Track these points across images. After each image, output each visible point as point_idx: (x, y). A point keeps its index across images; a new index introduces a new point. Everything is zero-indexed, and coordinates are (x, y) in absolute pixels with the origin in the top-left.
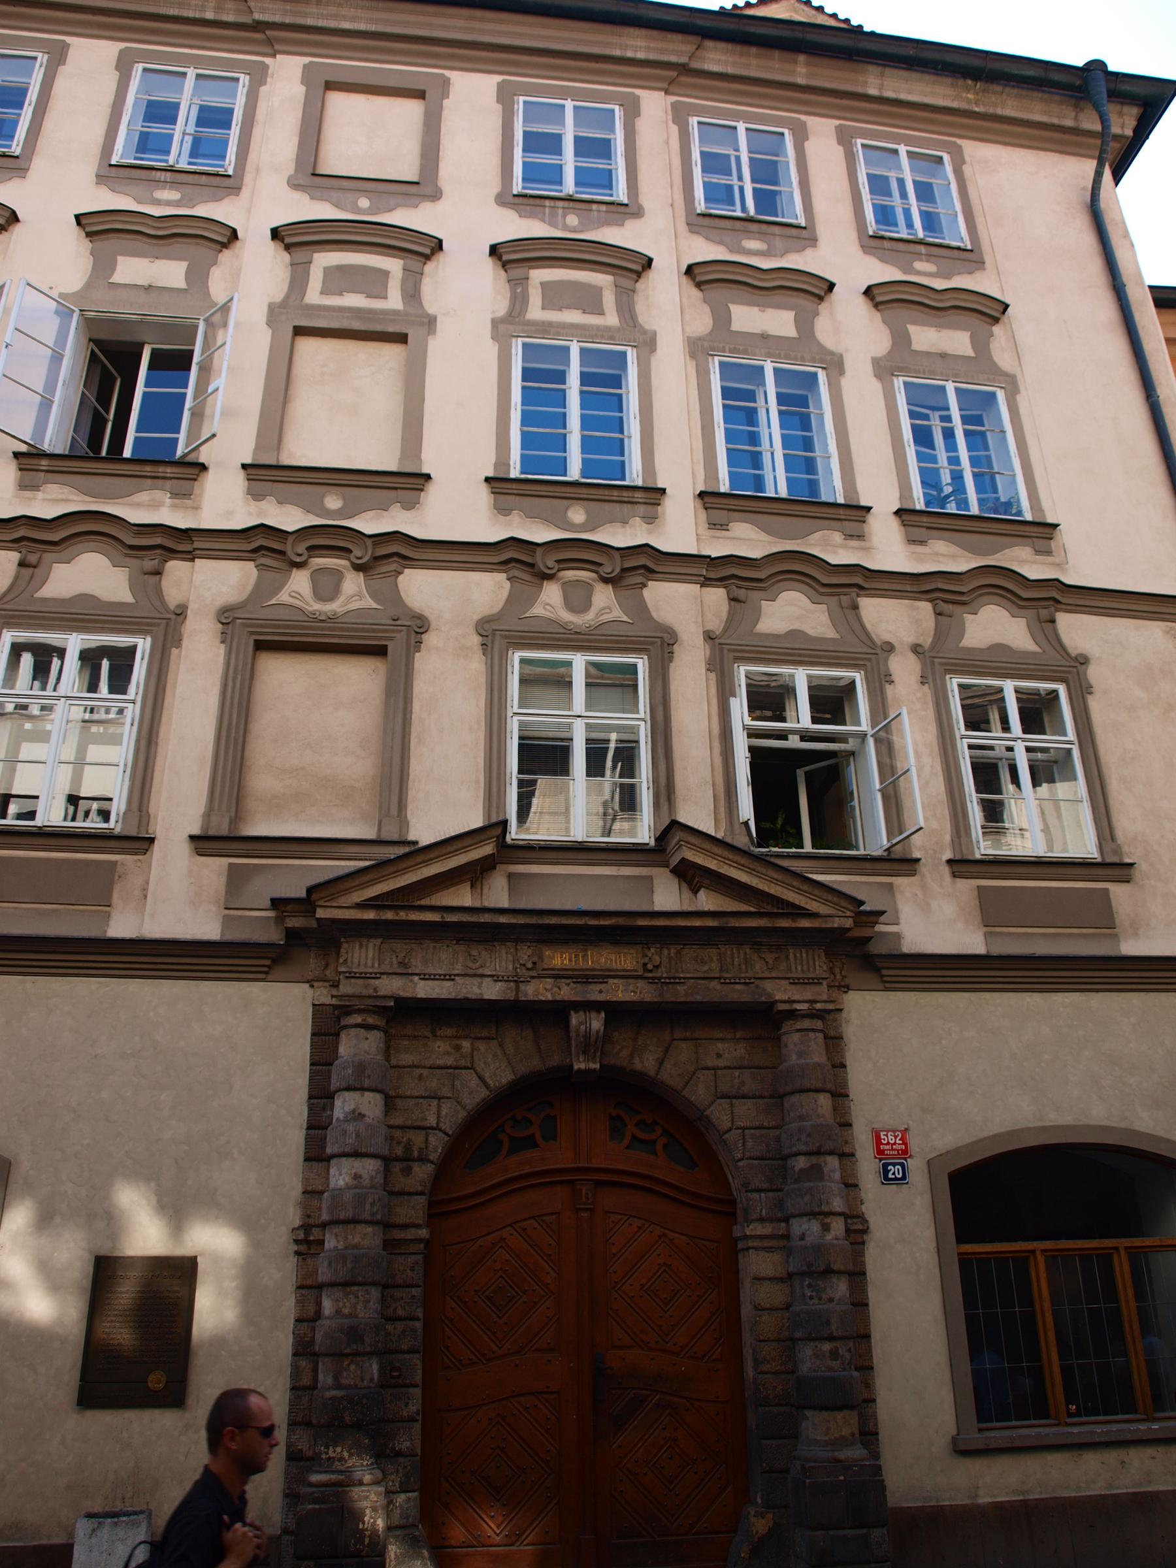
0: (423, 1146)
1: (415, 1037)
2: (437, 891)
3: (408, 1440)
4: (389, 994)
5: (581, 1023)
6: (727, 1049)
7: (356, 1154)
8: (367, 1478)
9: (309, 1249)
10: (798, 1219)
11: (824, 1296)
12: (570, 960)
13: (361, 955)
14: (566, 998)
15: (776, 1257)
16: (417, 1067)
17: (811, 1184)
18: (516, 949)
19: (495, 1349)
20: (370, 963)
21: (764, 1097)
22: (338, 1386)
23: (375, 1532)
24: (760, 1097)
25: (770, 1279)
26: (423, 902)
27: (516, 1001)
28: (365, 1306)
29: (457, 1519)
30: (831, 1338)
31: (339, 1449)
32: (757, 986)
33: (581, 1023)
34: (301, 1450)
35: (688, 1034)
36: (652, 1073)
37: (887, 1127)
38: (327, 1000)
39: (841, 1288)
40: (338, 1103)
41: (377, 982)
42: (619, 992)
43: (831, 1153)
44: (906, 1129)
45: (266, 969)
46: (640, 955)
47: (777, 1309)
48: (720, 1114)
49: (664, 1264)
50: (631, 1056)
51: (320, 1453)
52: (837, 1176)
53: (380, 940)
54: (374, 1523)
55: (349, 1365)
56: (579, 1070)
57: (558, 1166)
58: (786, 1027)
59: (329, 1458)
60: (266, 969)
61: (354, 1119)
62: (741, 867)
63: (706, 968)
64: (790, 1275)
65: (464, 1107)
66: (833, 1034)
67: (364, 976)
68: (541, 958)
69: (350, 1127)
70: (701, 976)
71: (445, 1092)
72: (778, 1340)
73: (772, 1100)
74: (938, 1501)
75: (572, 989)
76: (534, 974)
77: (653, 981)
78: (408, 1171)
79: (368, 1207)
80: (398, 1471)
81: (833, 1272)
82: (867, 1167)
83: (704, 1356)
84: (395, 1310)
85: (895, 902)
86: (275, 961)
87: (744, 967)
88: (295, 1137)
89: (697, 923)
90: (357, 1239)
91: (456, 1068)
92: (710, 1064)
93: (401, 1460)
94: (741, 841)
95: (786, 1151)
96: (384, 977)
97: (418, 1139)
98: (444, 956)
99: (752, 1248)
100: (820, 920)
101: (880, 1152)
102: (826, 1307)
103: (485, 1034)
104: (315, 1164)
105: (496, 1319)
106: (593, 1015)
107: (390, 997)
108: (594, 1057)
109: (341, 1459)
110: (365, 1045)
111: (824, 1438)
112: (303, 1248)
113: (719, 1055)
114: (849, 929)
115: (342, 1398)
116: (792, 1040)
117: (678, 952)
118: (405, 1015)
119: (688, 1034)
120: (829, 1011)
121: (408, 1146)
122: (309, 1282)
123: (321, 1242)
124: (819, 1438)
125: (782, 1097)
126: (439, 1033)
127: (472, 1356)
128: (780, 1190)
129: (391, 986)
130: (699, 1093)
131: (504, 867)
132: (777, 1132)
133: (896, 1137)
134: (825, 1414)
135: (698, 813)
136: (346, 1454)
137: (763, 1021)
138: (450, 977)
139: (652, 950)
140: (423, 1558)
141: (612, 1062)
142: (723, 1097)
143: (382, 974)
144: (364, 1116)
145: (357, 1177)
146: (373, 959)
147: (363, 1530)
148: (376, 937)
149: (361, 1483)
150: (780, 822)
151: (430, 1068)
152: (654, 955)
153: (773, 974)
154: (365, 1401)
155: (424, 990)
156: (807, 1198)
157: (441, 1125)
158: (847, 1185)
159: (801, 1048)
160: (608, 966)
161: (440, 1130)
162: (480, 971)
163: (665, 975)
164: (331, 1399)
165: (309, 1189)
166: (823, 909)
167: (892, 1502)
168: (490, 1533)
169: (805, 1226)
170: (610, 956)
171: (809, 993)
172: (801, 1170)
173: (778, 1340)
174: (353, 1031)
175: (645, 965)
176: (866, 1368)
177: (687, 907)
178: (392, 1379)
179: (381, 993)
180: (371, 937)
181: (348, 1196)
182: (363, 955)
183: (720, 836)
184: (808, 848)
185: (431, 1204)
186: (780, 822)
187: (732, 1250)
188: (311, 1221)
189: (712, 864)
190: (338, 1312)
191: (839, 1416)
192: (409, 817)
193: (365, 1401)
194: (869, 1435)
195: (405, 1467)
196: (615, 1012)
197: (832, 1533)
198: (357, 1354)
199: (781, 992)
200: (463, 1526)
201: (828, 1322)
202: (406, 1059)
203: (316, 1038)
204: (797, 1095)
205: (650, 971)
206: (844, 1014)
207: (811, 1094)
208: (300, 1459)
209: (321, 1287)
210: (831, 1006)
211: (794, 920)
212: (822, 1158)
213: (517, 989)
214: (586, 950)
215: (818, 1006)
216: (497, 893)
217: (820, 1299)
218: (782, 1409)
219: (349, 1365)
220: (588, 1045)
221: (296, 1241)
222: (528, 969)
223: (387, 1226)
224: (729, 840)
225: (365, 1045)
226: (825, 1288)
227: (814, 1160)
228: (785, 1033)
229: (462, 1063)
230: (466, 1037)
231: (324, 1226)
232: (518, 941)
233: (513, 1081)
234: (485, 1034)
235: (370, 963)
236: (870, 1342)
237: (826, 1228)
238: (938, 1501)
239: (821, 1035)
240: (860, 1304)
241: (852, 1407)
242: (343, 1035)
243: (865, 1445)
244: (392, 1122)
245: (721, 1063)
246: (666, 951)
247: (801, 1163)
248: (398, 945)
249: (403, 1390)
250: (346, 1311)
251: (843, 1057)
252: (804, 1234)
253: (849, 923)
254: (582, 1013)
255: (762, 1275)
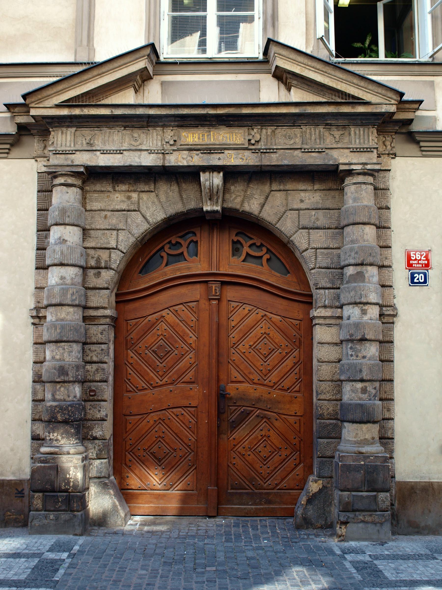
0: (108, 259)
1: (102, 191)
2: (110, 95)
3: (105, 430)
4: (82, 163)
5: (206, 180)
6: (308, 196)
7: (62, 265)
8: (72, 451)
9: (40, 321)
10: (347, 306)
11: (360, 355)
12: (199, 138)
13: (62, 139)
14: (196, 164)
15: (334, 330)
16: (103, 210)
17: (356, 284)
18: (163, 132)
19: (158, 381)
20: (68, 144)
21: (331, 229)
22: (54, 400)
23: (76, 480)
24: (329, 228)
25: (328, 343)
26: (103, 102)
27: (164, 167)
28: (71, 355)
29: (136, 475)
30: (362, 381)
31: (55, 434)
32: (327, 154)
33: (206, 180)
34: (39, 435)
35: (282, 187)
36: (256, 213)
37: (416, 249)
38: (44, 169)
39: (372, 350)
40: (52, 233)
41: (73, 156)
42: (232, 159)
43: (371, 265)
44: (430, 250)
45: (7, 151)
46: (247, 134)
47: (332, 362)
48: (300, 240)
49: (265, 333)
50: (243, 202)
51: (46, 436)
52: (375, 279)
53: (75, 129)
54: (75, 475)
55: (60, 388)
56: (207, 212)
57: (204, 272)
58: (348, 180)
59: (50, 439)
60: (7, 151)
61: (60, 243)
62: (317, 71)
63: (292, 142)
64: (342, 342)
65: (133, 235)
66: (382, 186)
67: (64, 153)
68: (179, 137)
69: (57, 248)
70: (288, 147)
71: (121, 226)
72: (332, 381)
73: (337, 230)
74: (429, 479)
75: (200, 158)
76: (175, 148)
77: (255, 151)
78: (98, 275)
79: (69, 296)
80: (95, 447)
81: (366, 340)
82: (400, 275)
83: (288, 389)
84: (92, 357)
85: (434, 94)
86: (12, 145)
87: (318, 141)
88: (30, 256)
89: (284, 110)
90: (63, 315)
91: (128, 211)
92: (295, 207)
93: (97, 441)
94: (323, 54)
95: (342, 264)
96: (78, 153)
97: (104, 255)
98: (116, 138)
99: (318, 324)
100: (372, 107)
101: (410, 265)
102: (360, 361)
103: (147, 188)
104: (41, 271)
105: (158, 363)
106: (215, 174)
107: (82, 165)
108: (217, 202)
109: (57, 440)
110: (66, 197)
111: (354, 439)
112: (36, 321)
113: (302, 201)
114: (393, 114)
115: (56, 406)
116: (350, 189)
117: (273, 132)
118: (92, 176)
119: (282, 187)
120: (378, 171)
121: (98, 260)
122: (40, 341)
123: (45, 317)
124: (351, 439)
125: (343, 228)
126: (117, 188)
127: (144, 385)
128: (339, 288)
129: (83, 159)
130: (286, 226)
131: (158, 77)
132: (339, 251)
133: (421, 256)
134: (355, 425)
135: (293, 34)
136: (59, 437)
137: (331, 177)
138: (120, 152)
139: (255, 130)
140: (110, 494)
141: (230, 205)
142: (303, 228)
143: (76, 151)
144: (66, 241)
145: (62, 278)
146: (70, 141)
147: (69, 478)
148: (71, 127)
149: (68, 453)
150: (367, 42)
151: (112, 211)
152: (256, 133)
153: (339, 146)
154: (70, 408)
155: (103, 161)
156: (352, 293)
157: (119, 246)
158: (383, 286)
159: (357, 196)
160: (224, 142)
161: (119, 250)
162: (140, 147)
163: (263, 148)
164: (49, 407)
165: (39, 286)
166: (374, 99)
167: (398, 478)
168: (155, 483)
169: (351, 311)
170: (226, 135)
171: (364, 158)
172: (350, 275)
173: (332, 381)
174: (59, 188)
175: (249, 140)
176: (387, 399)
177: (283, 100)
178: (91, 396)
179: (76, 163)
180: (68, 127)
181: (57, 290)
182: (64, 139)
183: (309, 52)
184: (382, 57)
185: (117, 295)
186: (367, 42)
187: (309, 325)
188: (40, 305)
189: (297, 69)
190: (53, 358)
191: (364, 427)
192: (95, 46)
193: (70, 408)
194: (386, 439)
195: (99, 446)
196: (231, 174)
197: (354, 493)
198: (64, 382)
199: (343, 158)
200: (139, 478)
201: (361, 371)
202: (96, 205)
203: (40, 194)
204: (351, 227)
205: (253, 145)
206: (391, 173)
207: (361, 226)
208: (39, 439)
209: (44, 343)
210: (377, 167)
211: (353, 108)
212: (364, 268)
213: (164, 159)
214: (210, 131)
215: (369, 167)
216: (153, 94)
217: (357, 356)
218: (332, 421)
219: (60, 388)
220: (212, 195)
221: (32, 317)
222: (171, 145)
223: (85, 308)
224: (315, 55)
225: (66, 197)
226: (361, 350)
227: (359, 269)
228: (347, 185)
229: (132, 207)
230: (135, 191)
231: (46, 307)
232: (164, 126)
233: (165, 218)
234: (147, 188)
235: (68, 144)
236: (393, 384)
237: (364, 312)
238: (429, 479)
239: (372, 187)
240: (387, 361)
241: (374, 422)
242: (54, 190)
243: (383, 444)
244: (88, 245)
245: (303, 206)
246: (264, 131)
247: (350, 271)
248: (87, 132)
249: (97, 403)
250: (58, 357)
251: (388, 202)
252: (349, 316)
253: (393, 109)
254: (207, 174)
255: (323, 341)
